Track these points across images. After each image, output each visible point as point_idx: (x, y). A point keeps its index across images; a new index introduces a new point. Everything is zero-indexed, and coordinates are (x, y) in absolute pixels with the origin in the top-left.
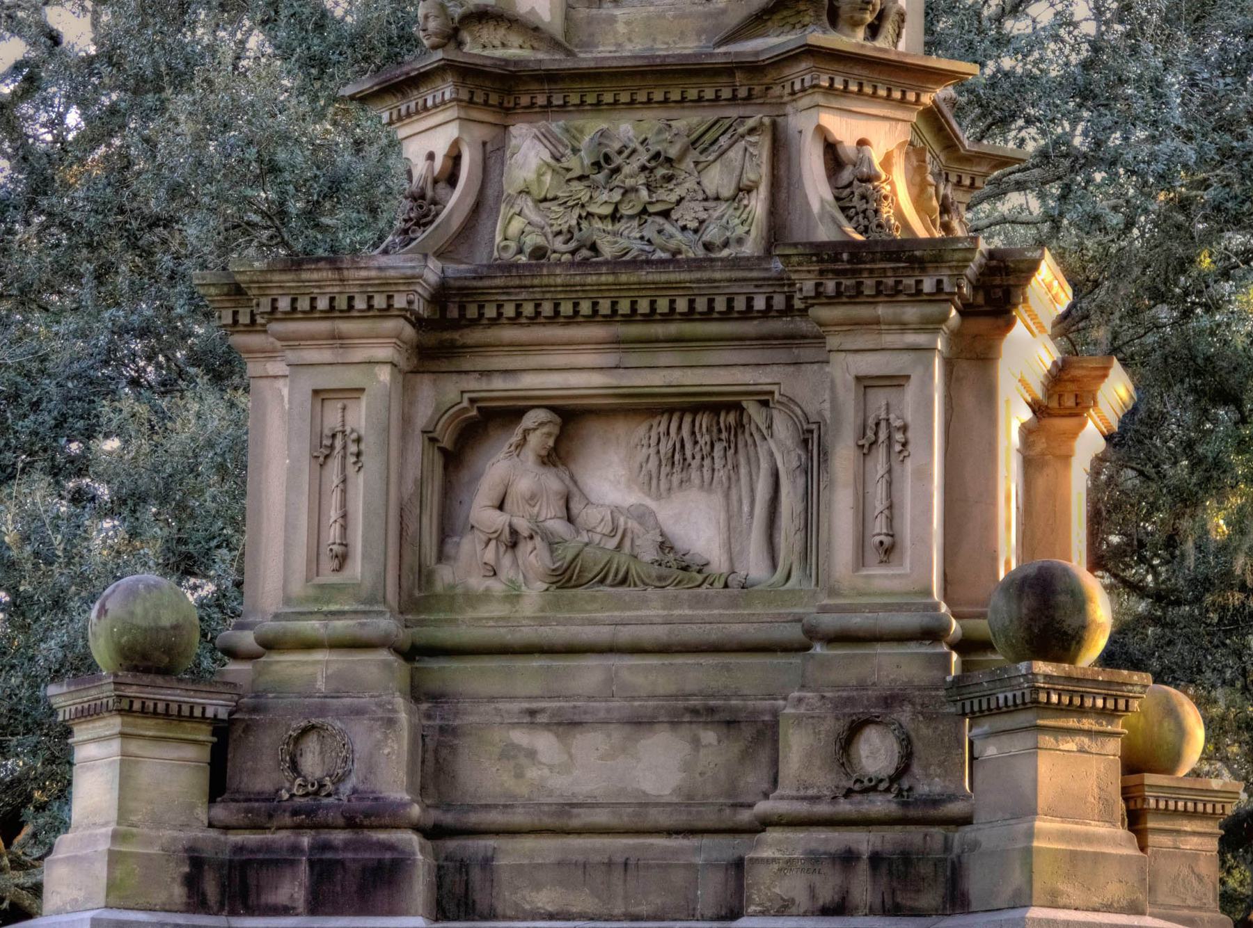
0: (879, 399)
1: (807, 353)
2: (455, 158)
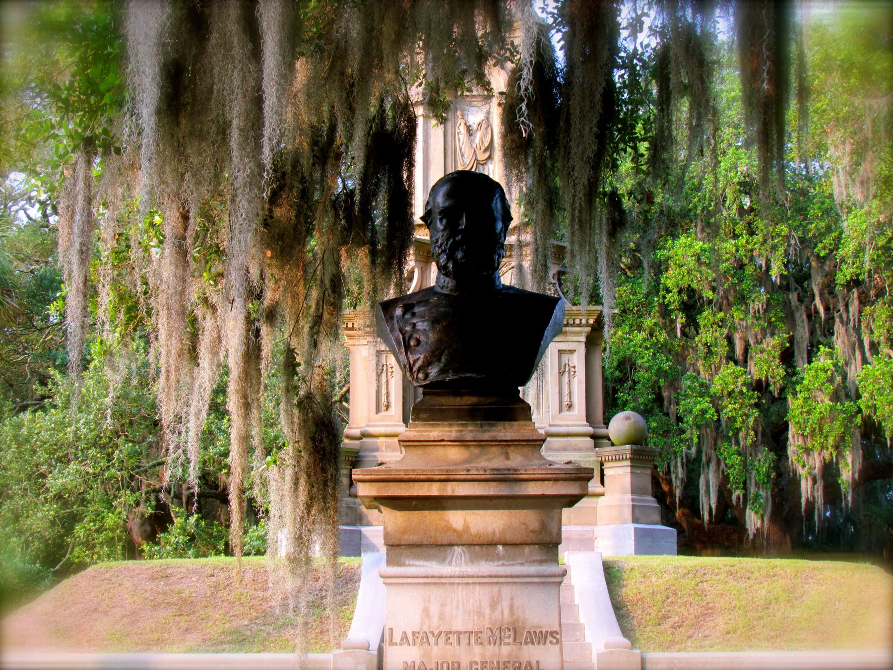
0: (565, 358)
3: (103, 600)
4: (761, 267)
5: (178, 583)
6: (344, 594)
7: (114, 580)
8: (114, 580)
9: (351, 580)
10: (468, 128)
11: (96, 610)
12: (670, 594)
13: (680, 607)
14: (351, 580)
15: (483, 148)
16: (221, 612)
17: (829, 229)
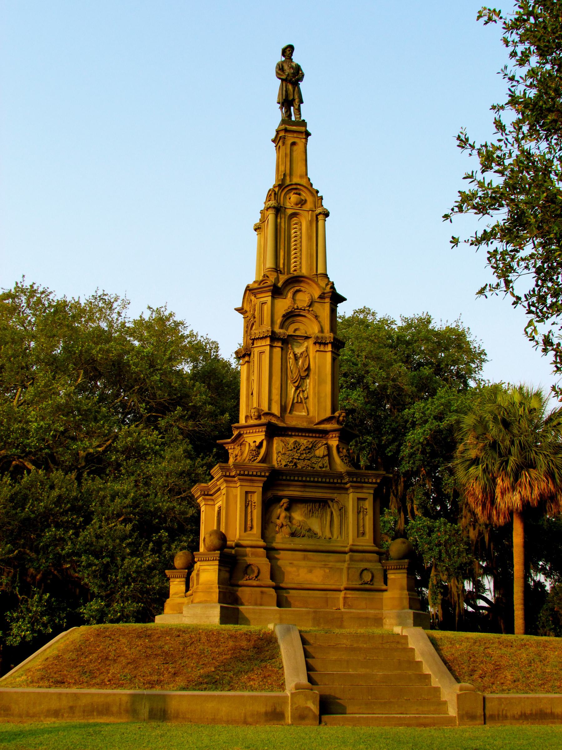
0: (361, 503)
1: (343, 492)
2: (261, 444)
3: (110, 651)
4: (354, 459)
5: (158, 641)
6: (270, 651)
7: (113, 637)
8: (113, 637)
9: (271, 642)
10: (295, 355)
11: (107, 658)
12: (472, 655)
13: (479, 664)
14: (271, 642)
15: (304, 369)
16: (193, 661)
17: (394, 440)
